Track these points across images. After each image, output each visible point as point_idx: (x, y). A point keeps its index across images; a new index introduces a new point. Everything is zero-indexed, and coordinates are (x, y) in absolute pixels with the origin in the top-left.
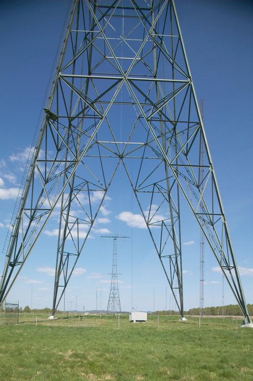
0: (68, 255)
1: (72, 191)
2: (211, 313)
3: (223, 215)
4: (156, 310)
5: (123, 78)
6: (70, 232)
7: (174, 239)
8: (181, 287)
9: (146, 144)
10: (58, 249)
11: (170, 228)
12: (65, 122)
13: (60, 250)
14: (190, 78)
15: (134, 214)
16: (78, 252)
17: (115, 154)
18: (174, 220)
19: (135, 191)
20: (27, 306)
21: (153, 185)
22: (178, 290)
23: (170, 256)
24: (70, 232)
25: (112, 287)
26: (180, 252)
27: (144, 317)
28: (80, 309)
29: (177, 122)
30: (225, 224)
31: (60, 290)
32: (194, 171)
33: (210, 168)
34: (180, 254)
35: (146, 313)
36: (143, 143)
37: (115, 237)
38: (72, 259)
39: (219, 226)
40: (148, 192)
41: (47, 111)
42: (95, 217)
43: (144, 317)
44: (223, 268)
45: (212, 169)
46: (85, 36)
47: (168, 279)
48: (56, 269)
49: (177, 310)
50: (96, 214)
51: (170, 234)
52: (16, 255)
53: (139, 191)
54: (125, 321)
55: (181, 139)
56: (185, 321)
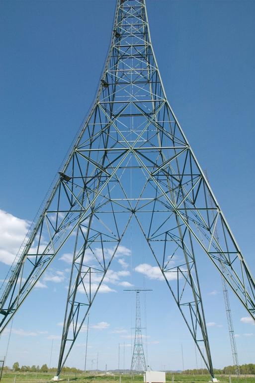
0: (79, 305)
1: (86, 242)
2: (250, 372)
3: (240, 253)
5: (130, 148)
6: (82, 281)
7: (192, 285)
8: (206, 340)
10: (69, 298)
12: (79, 182)
13: (71, 299)
15: (153, 266)
16: (90, 302)
17: (128, 209)
19: (148, 240)
20: (44, 364)
23: (190, 304)
24: (82, 281)
25: (136, 342)
26: (200, 299)
28: (102, 368)
29: (183, 175)
30: (243, 262)
31: (68, 344)
32: (202, 214)
33: (218, 210)
34: (201, 301)
35: (165, 373)
38: (83, 309)
39: (237, 265)
40: (162, 240)
41: (61, 174)
42: (109, 266)
43: (162, 378)
44: (250, 311)
47: (190, 331)
48: (65, 320)
49: (203, 366)
50: (110, 263)
52: (12, 302)
55: (185, 189)
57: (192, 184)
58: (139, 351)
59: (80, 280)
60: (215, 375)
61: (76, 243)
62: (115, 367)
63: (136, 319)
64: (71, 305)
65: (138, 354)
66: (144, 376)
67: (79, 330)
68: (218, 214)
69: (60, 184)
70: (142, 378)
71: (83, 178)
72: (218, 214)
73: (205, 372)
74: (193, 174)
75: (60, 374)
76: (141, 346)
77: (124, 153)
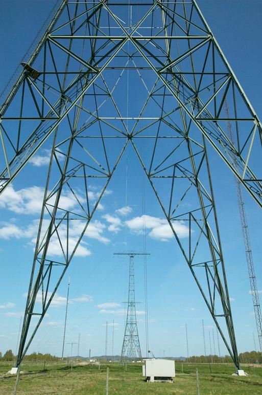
0: (51, 265)
4: (191, 355)
5: (127, 37)
6: (56, 230)
7: (208, 237)
8: (228, 314)
9: (160, 120)
11: (202, 224)
14: (210, 34)
18: (207, 210)
19: (149, 176)
21: (173, 166)
22: (224, 318)
23: (206, 264)
24: (56, 230)
27: (168, 369)
31: (35, 319)
33: (255, 122)
34: (222, 260)
36: (158, 118)
37: (132, 254)
38: (57, 271)
41: (27, 67)
43: (168, 369)
45: (258, 122)
46: (86, 18)
47: (206, 301)
48: (31, 285)
49: (224, 352)
51: (202, 231)
53: (155, 175)
54: (132, 378)
56: (245, 377)
57: (215, 89)
58: (131, 332)
59: (54, 228)
60: (241, 365)
61: (49, 176)
62: (100, 353)
63: (130, 290)
64: (40, 265)
65: (131, 336)
66: (144, 366)
67: (50, 300)
68: (256, 126)
69: (24, 80)
70: (139, 369)
71: (57, 73)
72: (256, 126)
73: (226, 359)
74: (216, 72)
75: (22, 364)
76: (134, 325)
77: (122, 41)
